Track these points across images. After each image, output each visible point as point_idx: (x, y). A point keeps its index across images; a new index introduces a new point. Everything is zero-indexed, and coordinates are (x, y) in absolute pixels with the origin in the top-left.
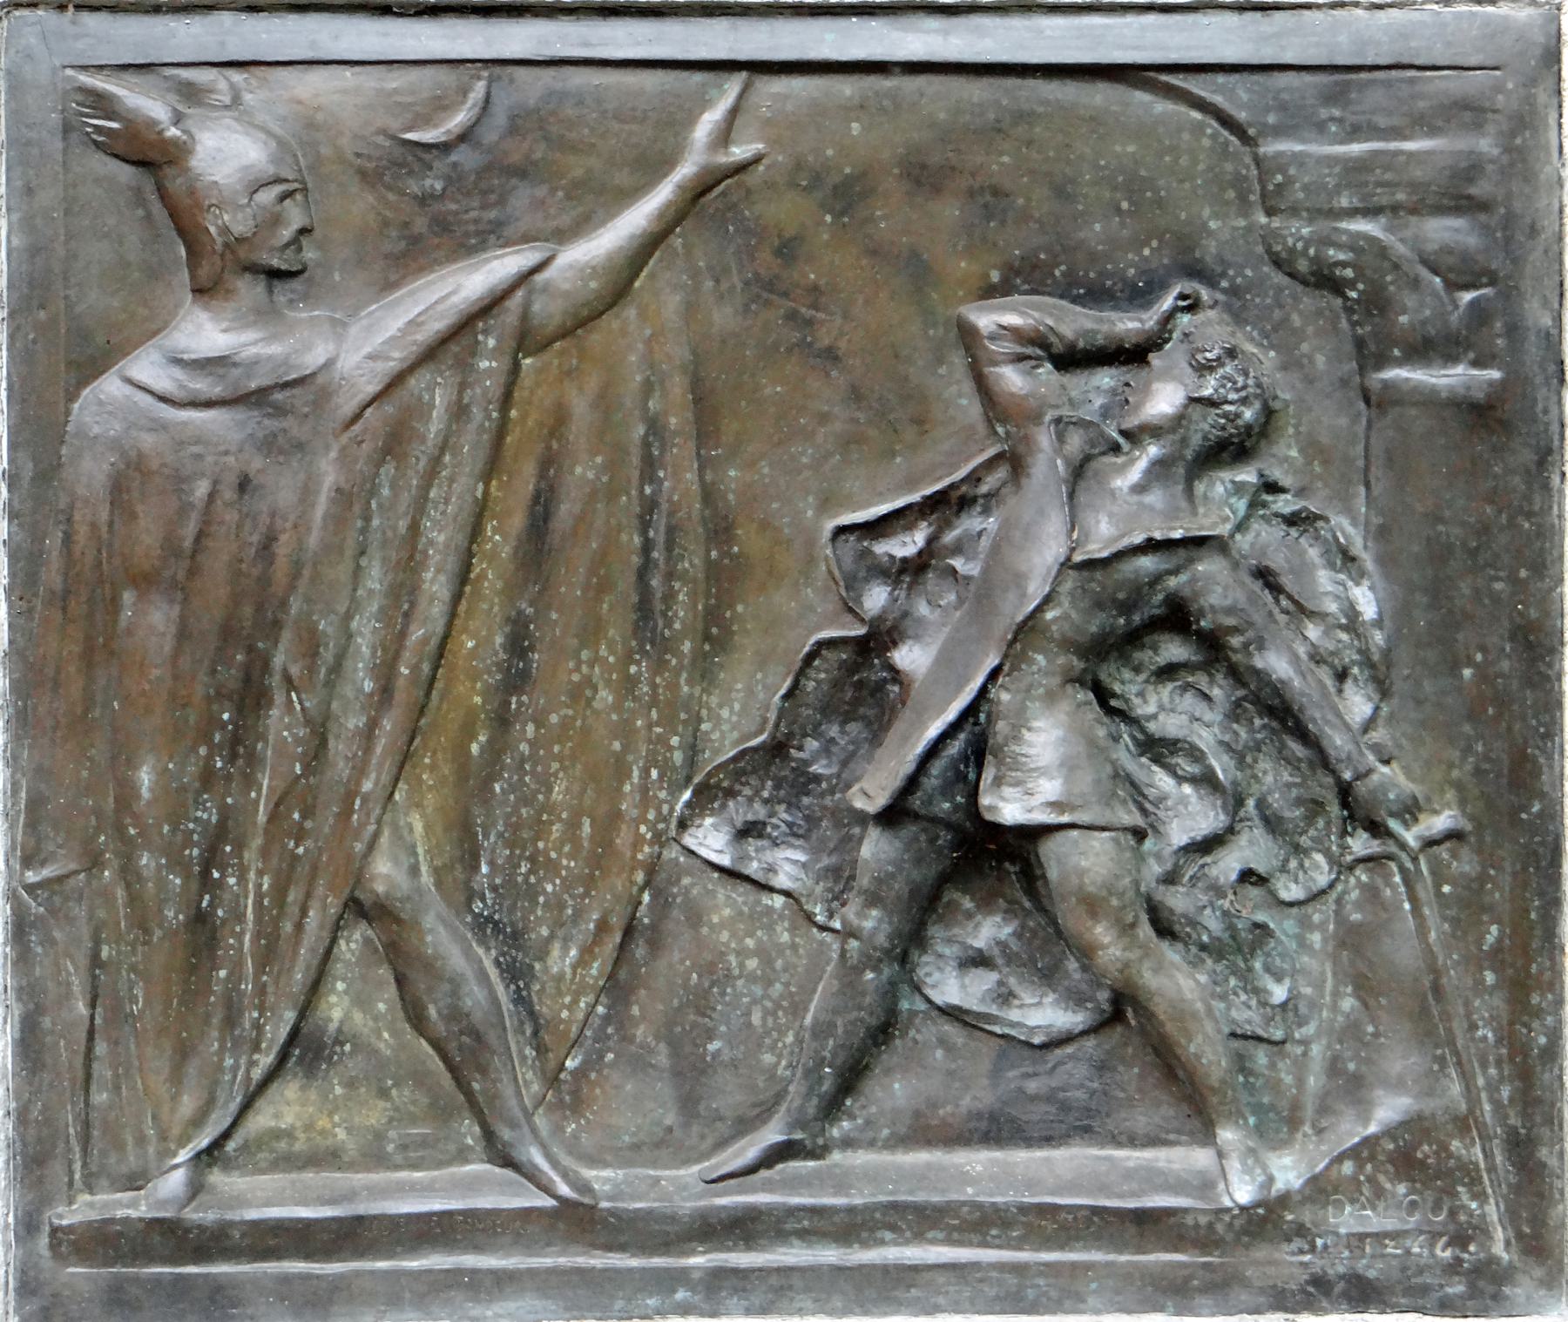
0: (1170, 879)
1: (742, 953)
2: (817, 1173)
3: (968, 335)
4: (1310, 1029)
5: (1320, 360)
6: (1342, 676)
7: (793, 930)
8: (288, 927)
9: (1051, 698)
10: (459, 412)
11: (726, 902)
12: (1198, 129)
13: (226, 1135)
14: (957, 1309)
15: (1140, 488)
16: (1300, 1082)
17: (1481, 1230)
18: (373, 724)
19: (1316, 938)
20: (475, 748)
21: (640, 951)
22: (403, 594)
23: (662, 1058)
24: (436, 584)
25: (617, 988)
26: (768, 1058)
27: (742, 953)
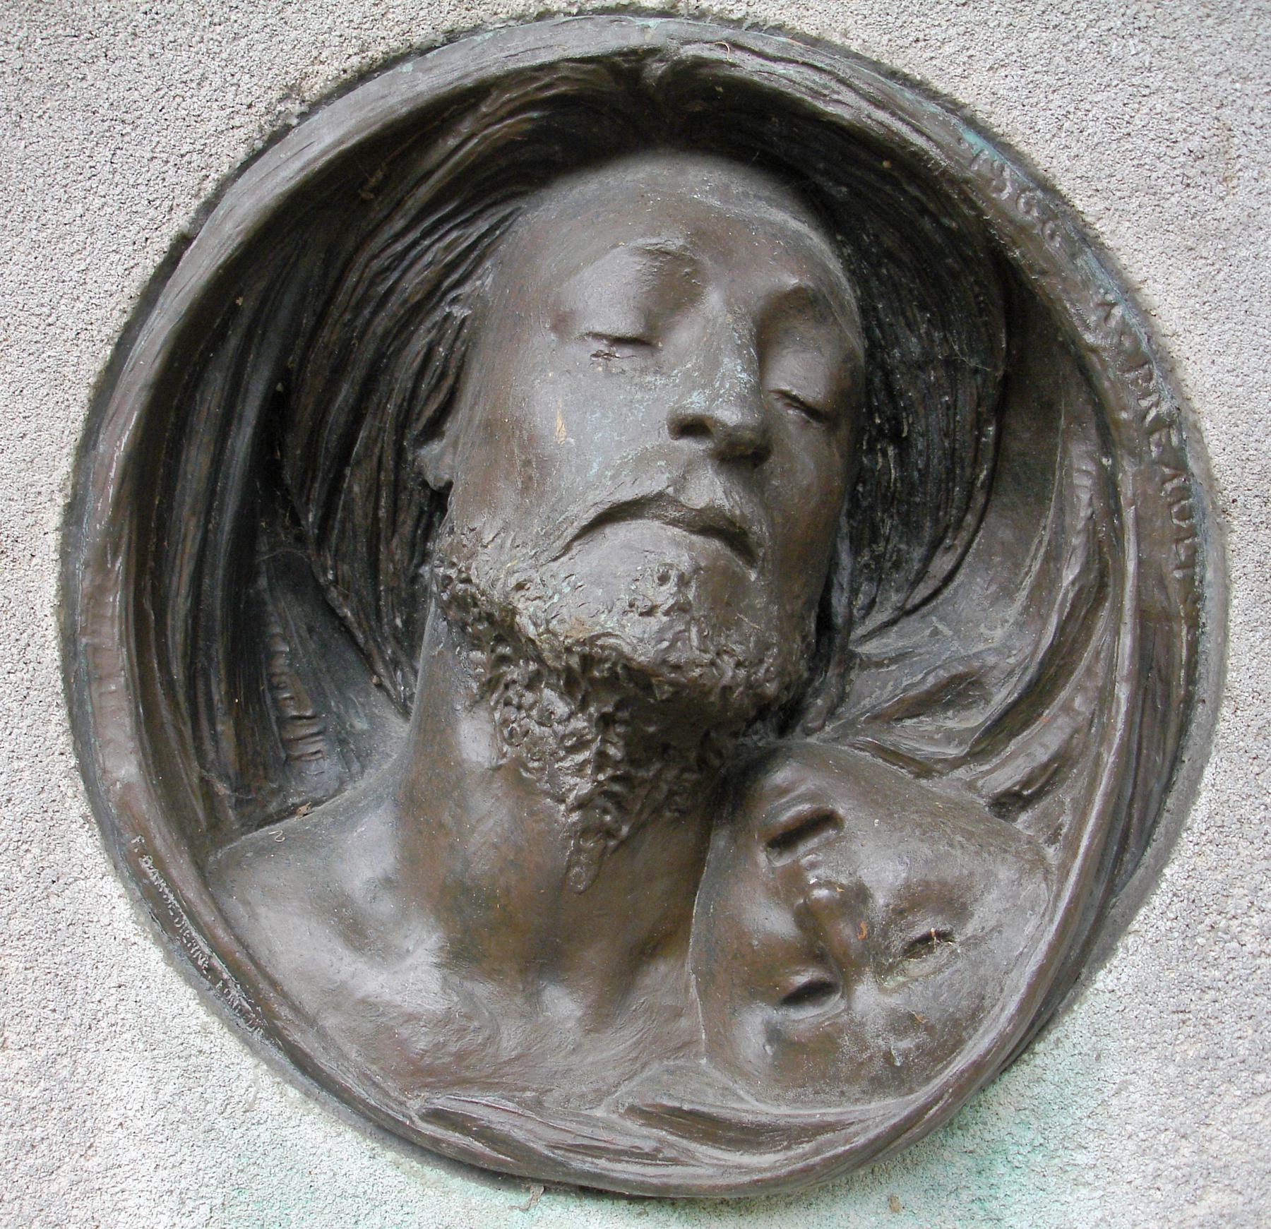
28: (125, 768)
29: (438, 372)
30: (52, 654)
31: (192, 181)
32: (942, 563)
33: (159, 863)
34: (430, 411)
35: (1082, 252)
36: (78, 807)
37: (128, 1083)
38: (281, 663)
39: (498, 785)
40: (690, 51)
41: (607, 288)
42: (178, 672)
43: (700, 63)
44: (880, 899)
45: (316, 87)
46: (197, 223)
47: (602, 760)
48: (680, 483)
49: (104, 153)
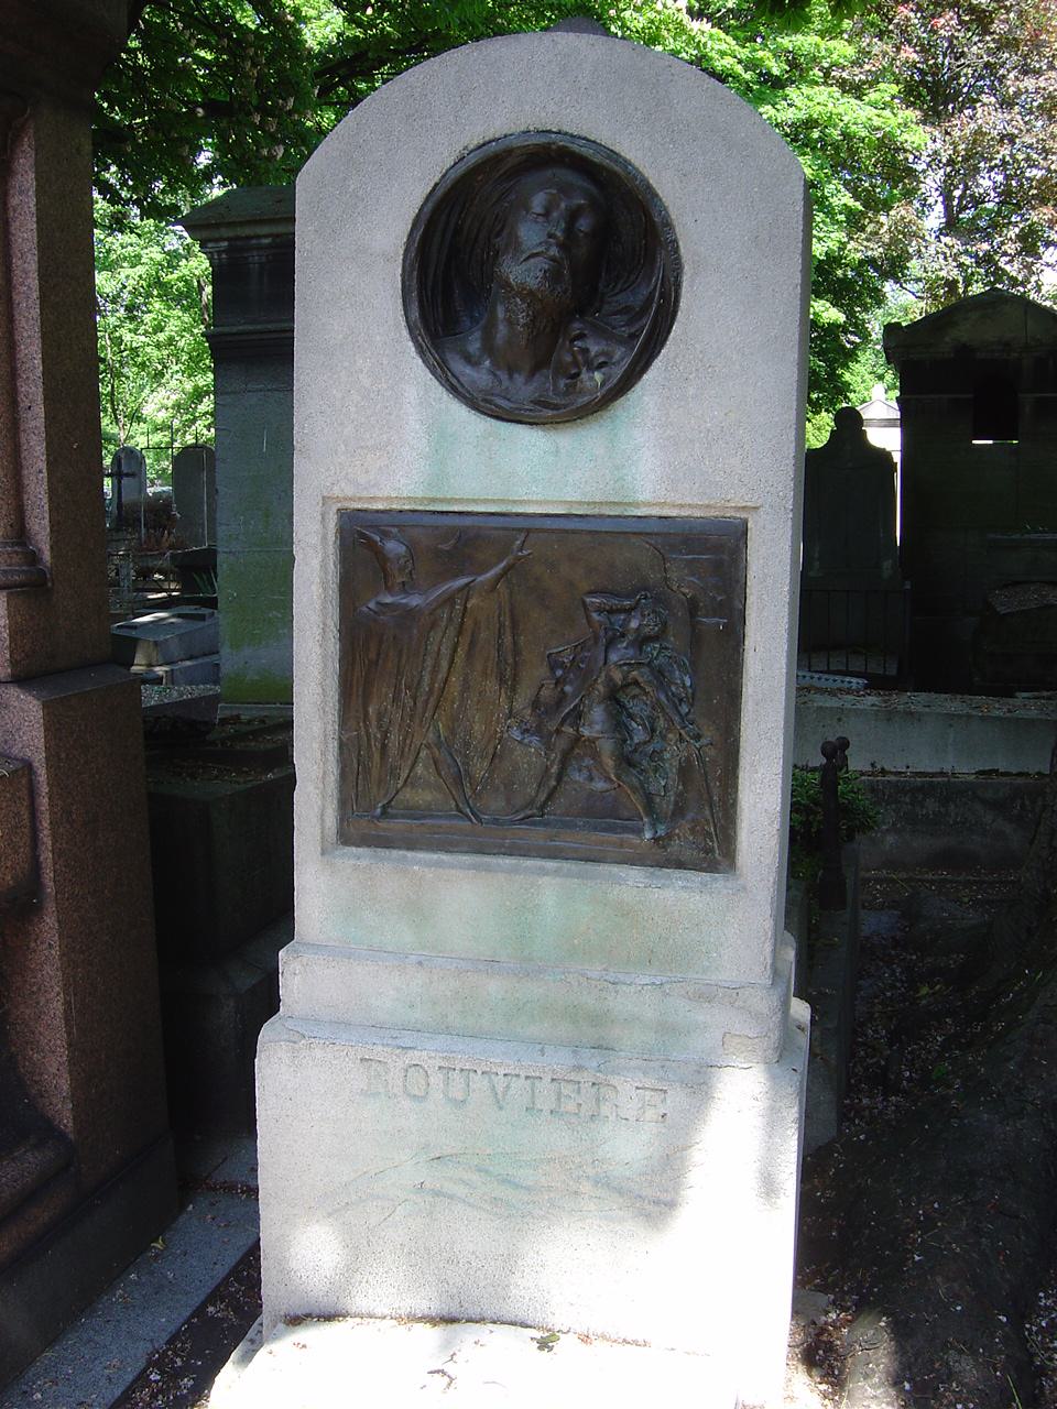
0: (635, 750)
1: (524, 763)
2: (540, 821)
3: (584, 602)
4: (672, 793)
5: (680, 614)
6: (681, 700)
7: (585, 779)
8: (407, 749)
9: (599, 703)
10: (450, 619)
11: (519, 750)
12: (648, 550)
13: (392, 800)
14: (16, 633)
15: (626, 648)
16: (668, 806)
17: (712, 850)
18: (428, 699)
19: (674, 770)
20: (156, 576)
21: (497, 761)
22: (436, 666)
23: (502, 788)
24: (444, 664)
25: (491, 770)
26: (529, 790)
27: (524, 763)
28: (415, 314)
29: (187, 610)
30: (400, 286)
31: (440, 170)
32: (632, 277)
33: (422, 338)
34: (498, 229)
35: (185, 309)
36: (404, 324)
37: (411, 393)
38: (456, 295)
39: (505, 323)
40: (561, 143)
41: (538, 202)
42: (429, 294)
43: (563, 146)
44: (593, 354)
45: (471, 147)
46: (441, 180)
47: (528, 315)
48: (547, 250)
49: (418, 161)
